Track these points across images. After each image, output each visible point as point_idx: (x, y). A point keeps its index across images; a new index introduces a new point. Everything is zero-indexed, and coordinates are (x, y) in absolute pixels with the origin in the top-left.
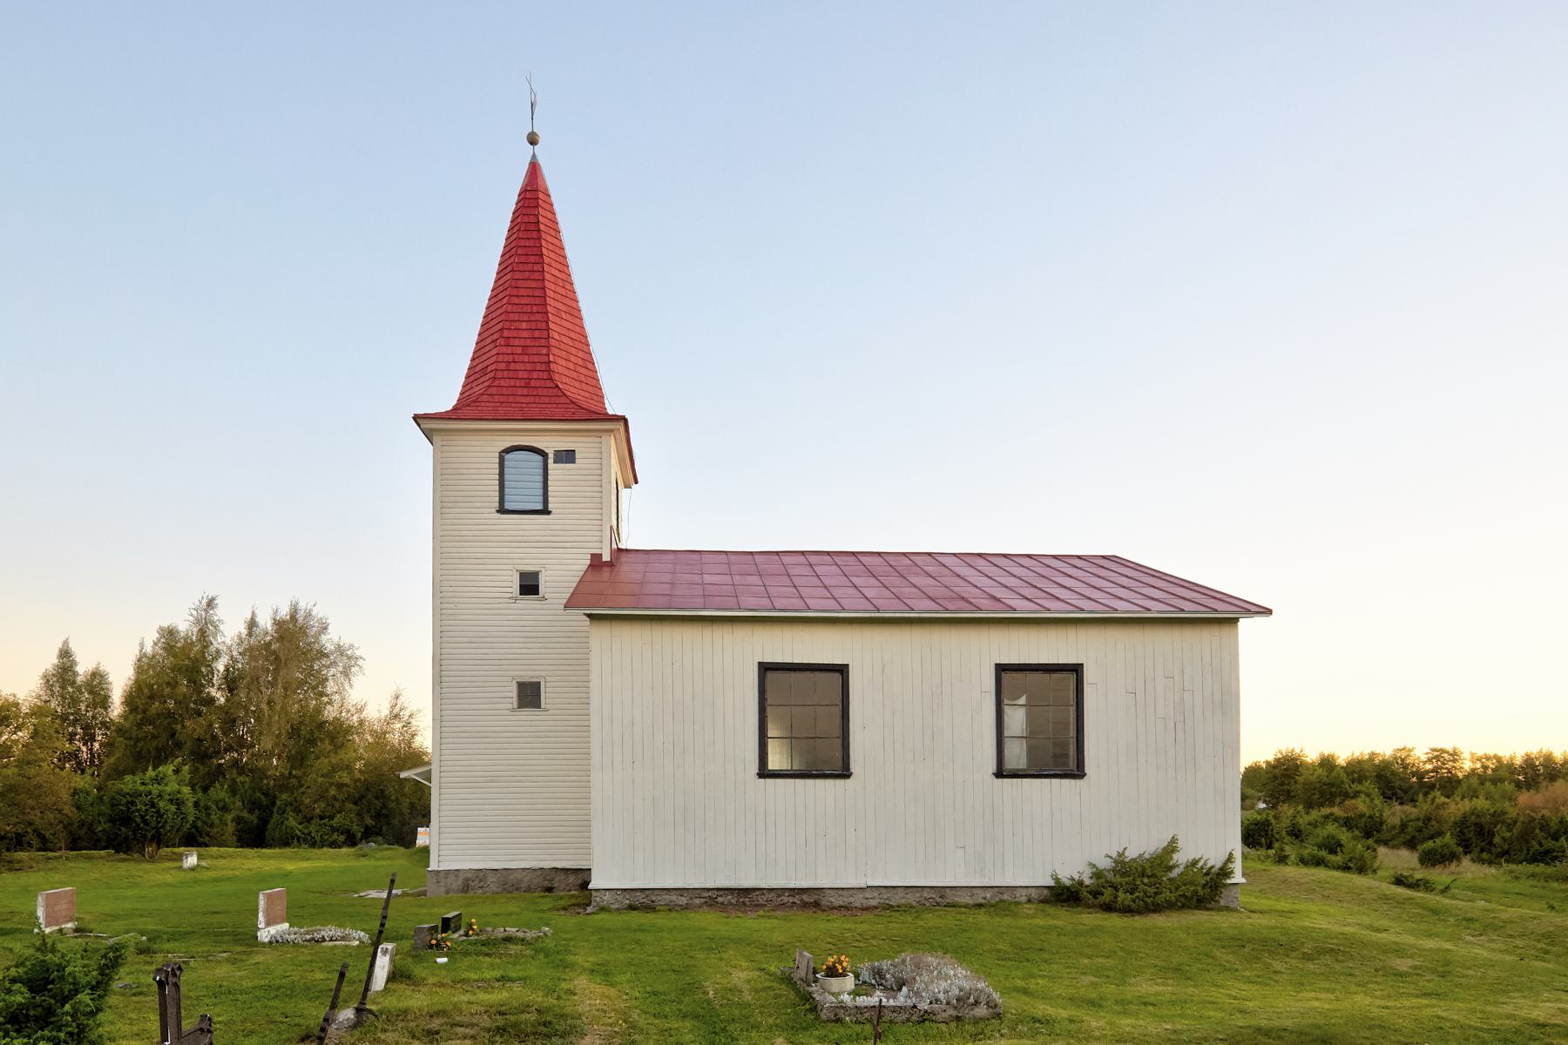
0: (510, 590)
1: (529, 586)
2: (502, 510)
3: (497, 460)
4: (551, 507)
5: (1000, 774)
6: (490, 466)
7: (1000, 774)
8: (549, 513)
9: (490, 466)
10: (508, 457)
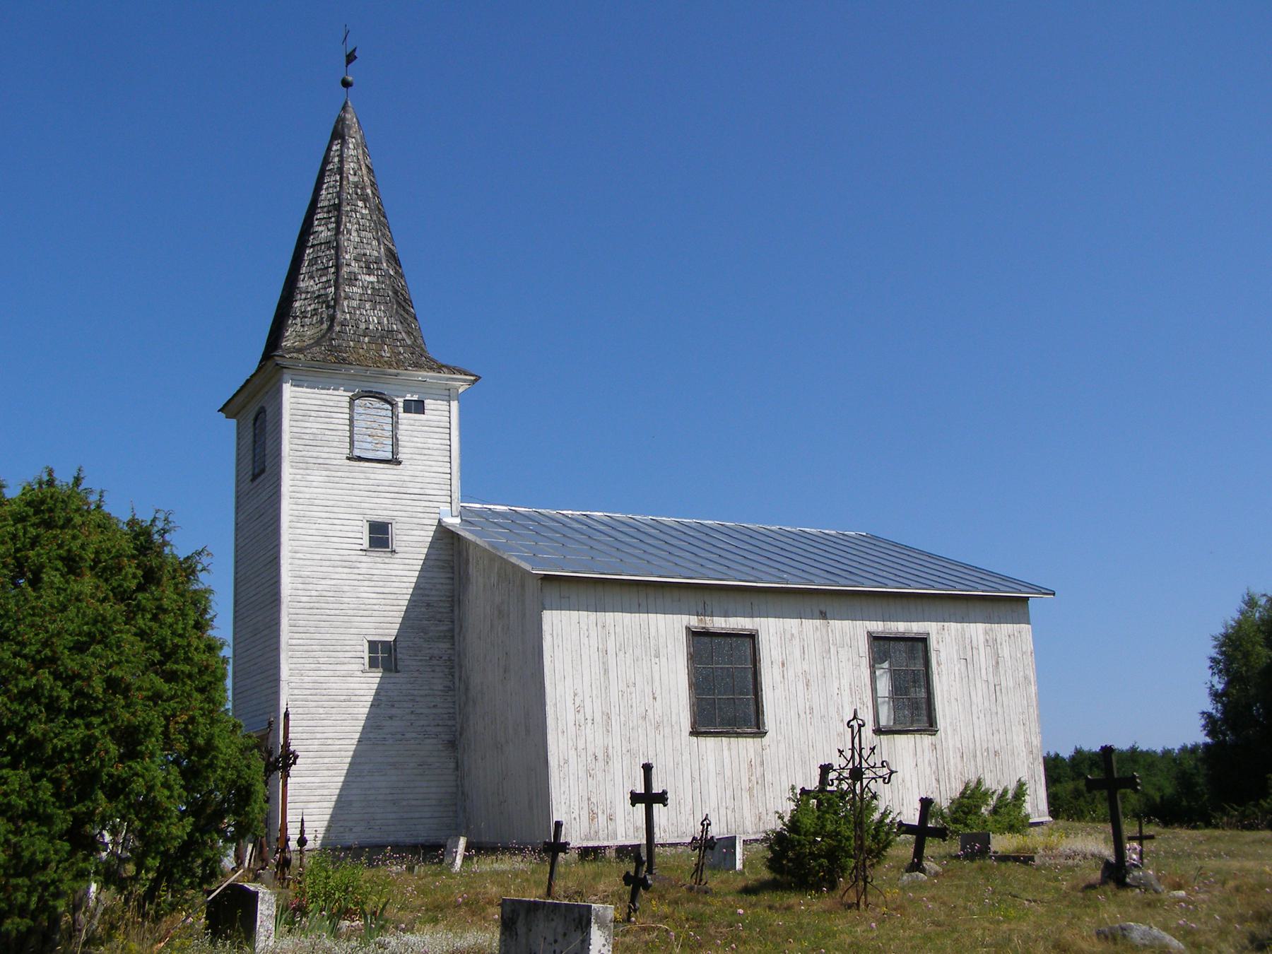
0: (360, 541)
1: (380, 535)
6: (341, 421)
8: (400, 463)
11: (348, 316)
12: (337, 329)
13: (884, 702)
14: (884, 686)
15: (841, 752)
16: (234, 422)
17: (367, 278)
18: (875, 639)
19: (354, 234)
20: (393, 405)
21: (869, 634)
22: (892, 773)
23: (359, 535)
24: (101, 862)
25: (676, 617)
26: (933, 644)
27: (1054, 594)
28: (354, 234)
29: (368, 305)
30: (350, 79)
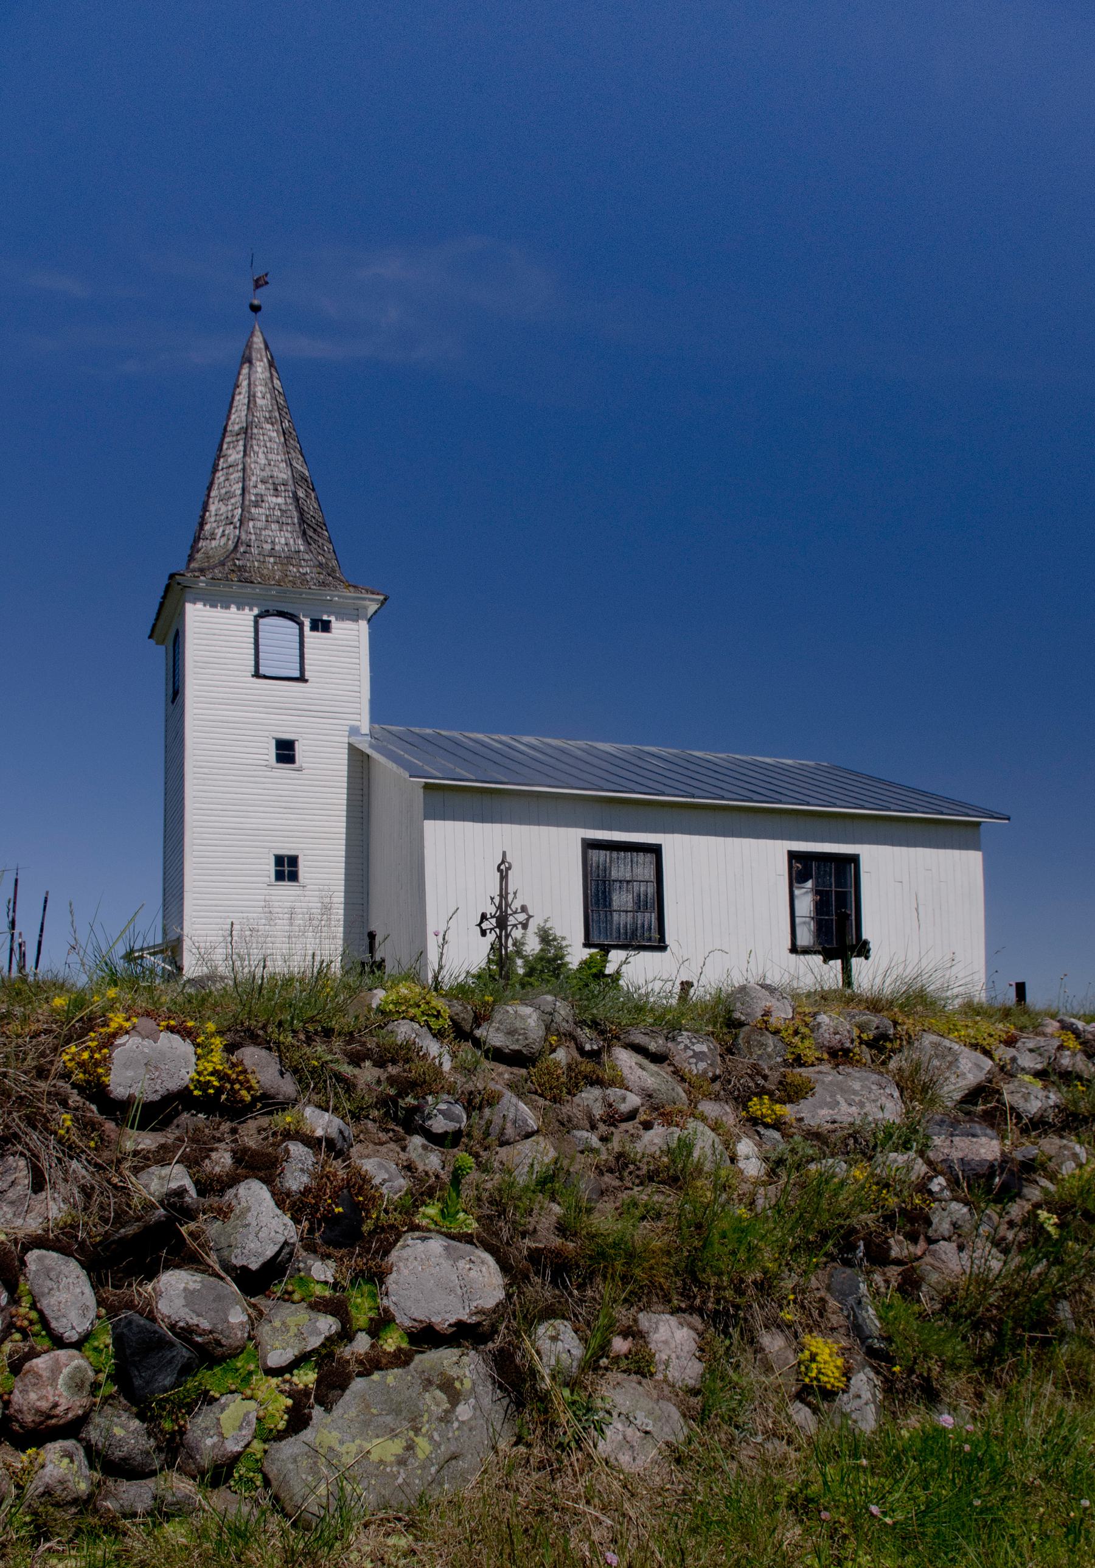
0: (266, 757)
1: (285, 751)
2: (257, 675)
3: (252, 623)
4: (307, 675)
5: (794, 950)
7: (794, 950)
8: (306, 681)
9: (269, 642)
10: (261, 621)
11: (253, 537)
12: (242, 549)
13: (804, 923)
14: (806, 904)
15: (492, 899)
16: (163, 647)
17: (274, 499)
18: (793, 856)
19: (261, 455)
20: (301, 625)
21: (584, 840)
22: (530, 917)
23: (266, 751)
24: (272, 553)
25: (779, 842)
26: (864, 866)
27: (1009, 819)
28: (261, 455)
29: (274, 526)
30: (256, 302)
